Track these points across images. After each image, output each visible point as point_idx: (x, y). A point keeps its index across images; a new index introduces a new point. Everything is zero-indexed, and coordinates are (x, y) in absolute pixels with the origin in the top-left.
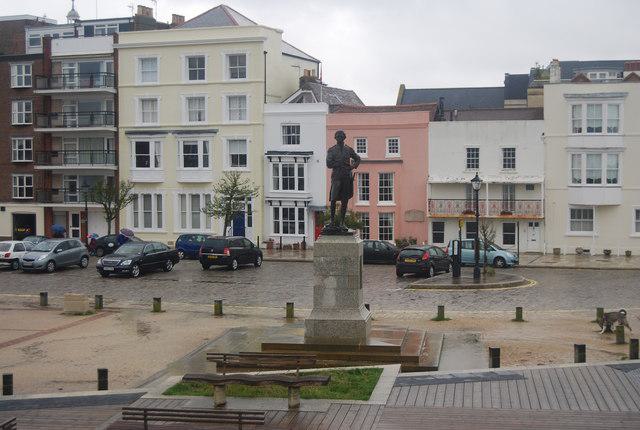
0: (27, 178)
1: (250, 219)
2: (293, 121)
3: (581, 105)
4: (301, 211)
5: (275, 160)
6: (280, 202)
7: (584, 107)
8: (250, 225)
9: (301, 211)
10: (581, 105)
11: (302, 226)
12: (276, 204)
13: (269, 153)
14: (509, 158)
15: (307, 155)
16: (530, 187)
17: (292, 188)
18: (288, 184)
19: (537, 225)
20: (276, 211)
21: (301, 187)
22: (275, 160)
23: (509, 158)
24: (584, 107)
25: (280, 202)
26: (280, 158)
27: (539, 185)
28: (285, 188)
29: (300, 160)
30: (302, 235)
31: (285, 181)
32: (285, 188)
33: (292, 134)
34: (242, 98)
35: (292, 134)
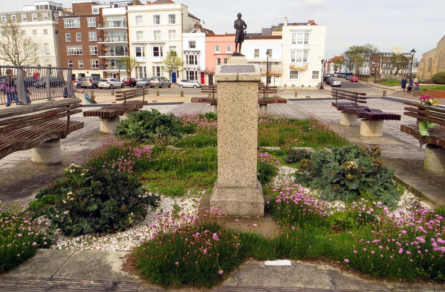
1: (178, 75)
2: (193, 39)
3: (295, 34)
4: (196, 72)
5: (187, 54)
7: (297, 34)
8: (178, 77)
9: (196, 72)
10: (295, 34)
11: (196, 78)
12: (187, 70)
14: (269, 52)
15: (198, 52)
16: (277, 63)
17: (193, 64)
18: (192, 63)
19: (278, 77)
20: (187, 72)
21: (196, 63)
22: (187, 54)
23: (269, 52)
24: (297, 34)
27: (280, 62)
28: (190, 64)
29: (196, 54)
31: (190, 61)
32: (190, 64)
33: (192, 45)
34: (174, 31)
35: (192, 45)
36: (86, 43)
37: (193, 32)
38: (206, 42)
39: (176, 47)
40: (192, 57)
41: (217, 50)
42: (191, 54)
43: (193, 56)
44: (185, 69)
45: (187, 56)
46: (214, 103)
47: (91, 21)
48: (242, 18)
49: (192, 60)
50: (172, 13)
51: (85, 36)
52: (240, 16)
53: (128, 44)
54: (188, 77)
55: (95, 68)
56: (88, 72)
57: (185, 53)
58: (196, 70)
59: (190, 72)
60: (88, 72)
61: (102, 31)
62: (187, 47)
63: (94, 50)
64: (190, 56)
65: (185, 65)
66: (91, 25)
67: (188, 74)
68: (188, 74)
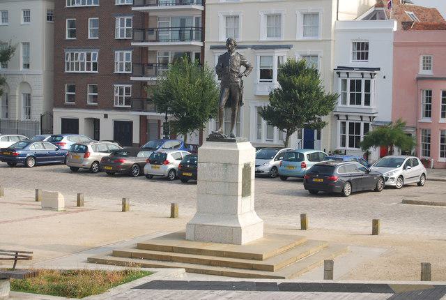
6: (347, 116)
8: (319, 138)
18: (355, 99)
21: (367, 102)
25: (361, 117)
26: (348, 73)
28: (352, 103)
29: (367, 76)
32: (352, 103)
36: (108, 45)
40: (355, 85)
41: (427, 67)
42: (355, 75)
43: (359, 82)
45: (345, 81)
46: (433, 168)
47: (122, 59)
49: (359, 91)
51: (107, 28)
53: (203, 48)
54: (344, 138)
55: (124, 106)
56: (106, 116)
58: (366, 120)
59: (351, 124)
60: (106, 116)
61: (145, 15)
63: (125, 27)
65: (339, 106)
66: (122, 35)
67: (344, 131)
68: (344, 131)
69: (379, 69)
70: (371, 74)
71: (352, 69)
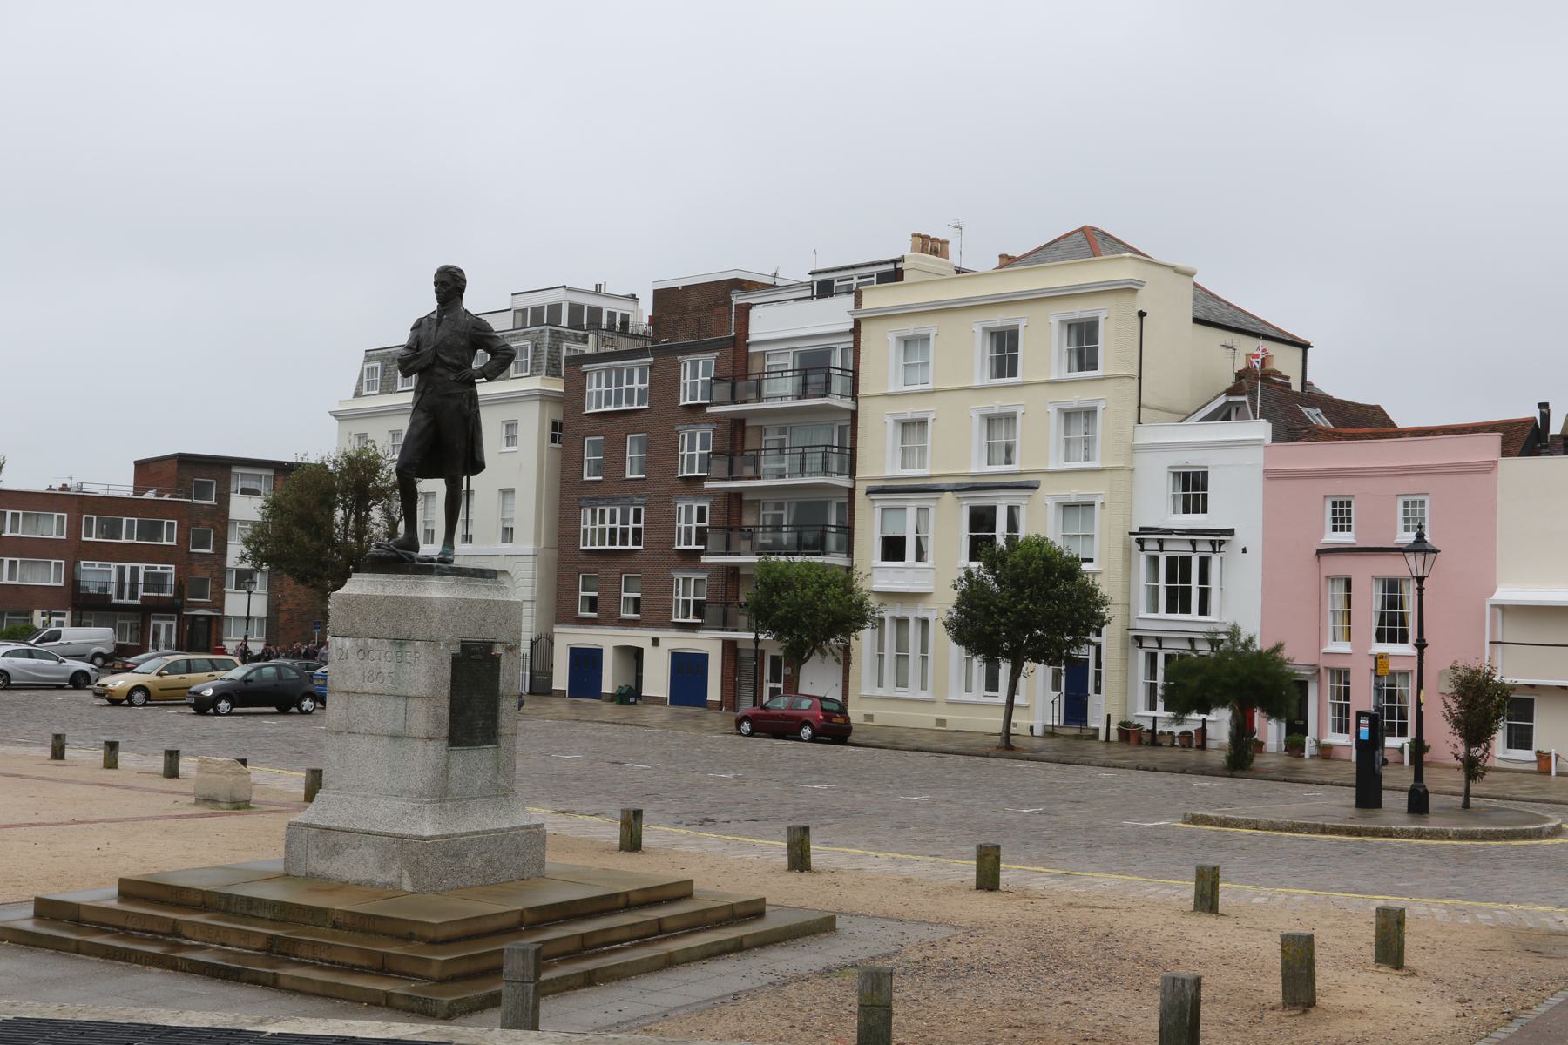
0: (1188, 611)
2: (1193, 460)
5: (1152, 547)
6: (1159, 640)
8: (1098, 690)
12: (1151, 645)
13: (1144, 530)
15: (1219, 538)
18: (1178, 601)
21: (1203, 610)
22: (1152, 547)
26: (1161, 542)
29: (1204, 548)
30: (1153, 713)
31: (1171, 593)
33: (1192, 488)
34: (1090, 413)
37: (1211, 417)
38: (1271, 476)
39: (1092, 505)
43: (1186, 561)
44: (1139, 639)
45: (1154, 560)
48: (472, 302)
49: (1182, 583)
50: (1079, 311)
52: (450, 284)
57: (1141, 542)
62: (1159, 507)
64: (1171, 561)
67: (1153, 672)
68: (1153, 672)
69: (1231, 532)
70: (1212, 543)
71: (1170, 531)
